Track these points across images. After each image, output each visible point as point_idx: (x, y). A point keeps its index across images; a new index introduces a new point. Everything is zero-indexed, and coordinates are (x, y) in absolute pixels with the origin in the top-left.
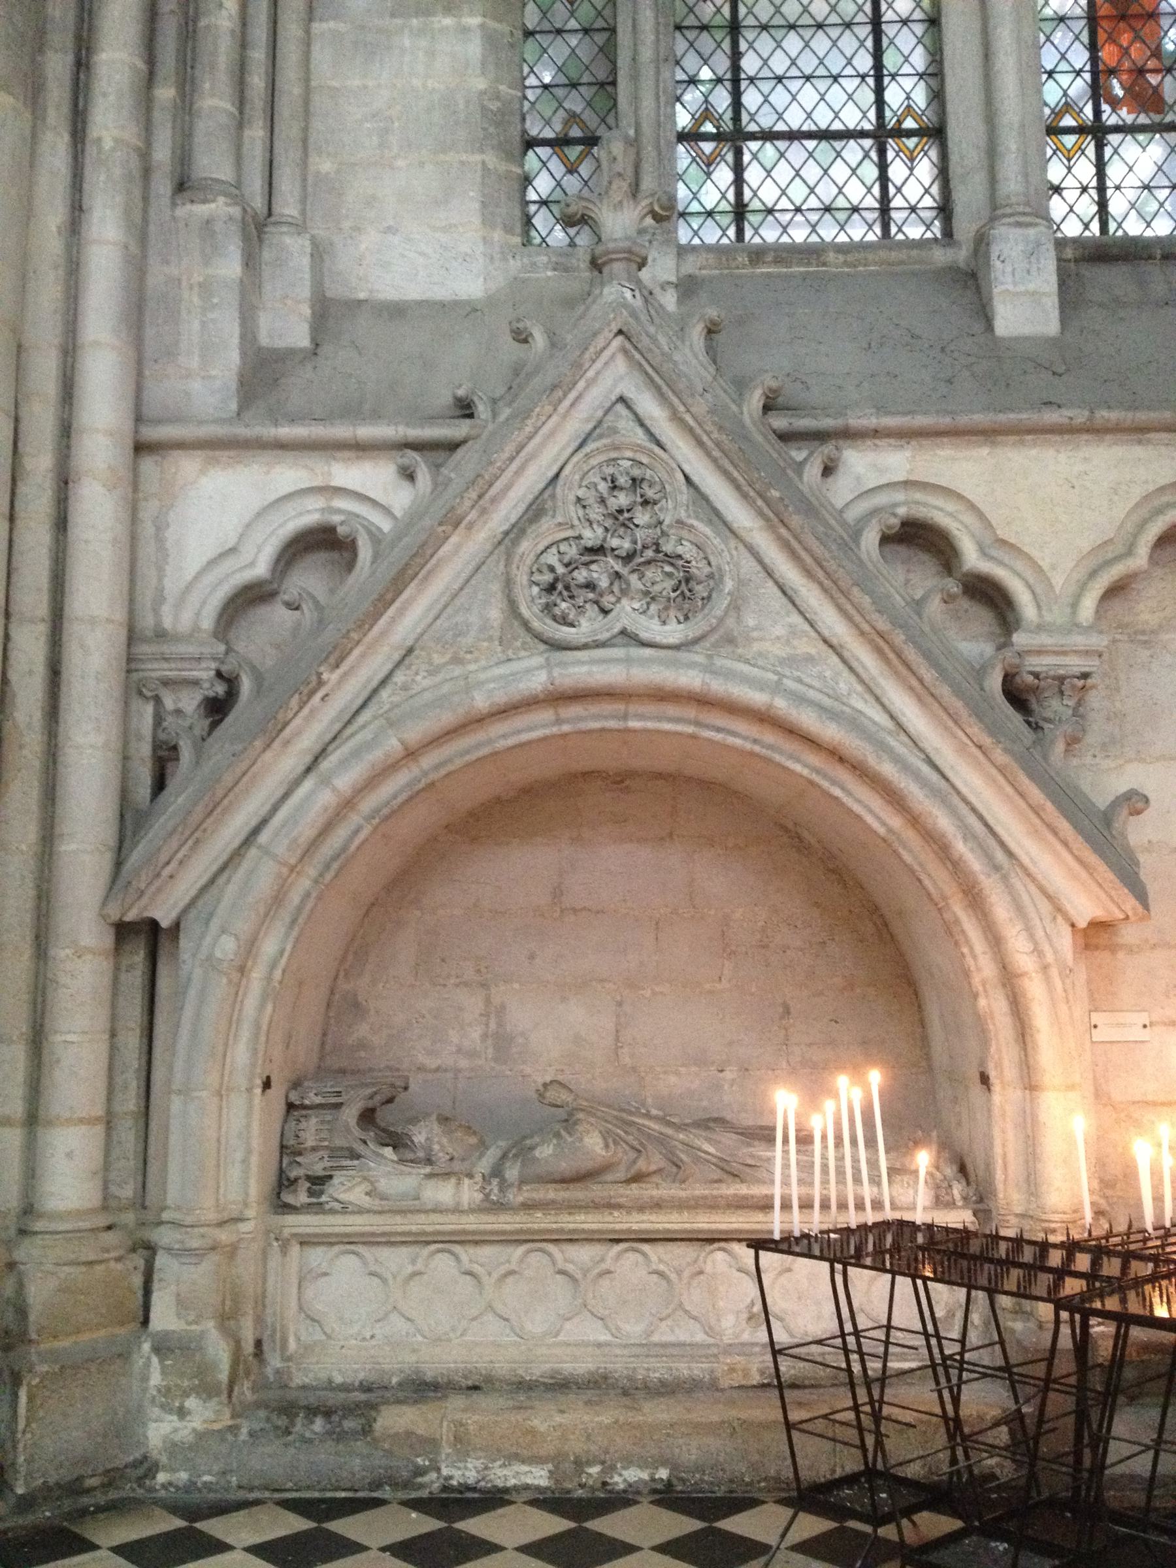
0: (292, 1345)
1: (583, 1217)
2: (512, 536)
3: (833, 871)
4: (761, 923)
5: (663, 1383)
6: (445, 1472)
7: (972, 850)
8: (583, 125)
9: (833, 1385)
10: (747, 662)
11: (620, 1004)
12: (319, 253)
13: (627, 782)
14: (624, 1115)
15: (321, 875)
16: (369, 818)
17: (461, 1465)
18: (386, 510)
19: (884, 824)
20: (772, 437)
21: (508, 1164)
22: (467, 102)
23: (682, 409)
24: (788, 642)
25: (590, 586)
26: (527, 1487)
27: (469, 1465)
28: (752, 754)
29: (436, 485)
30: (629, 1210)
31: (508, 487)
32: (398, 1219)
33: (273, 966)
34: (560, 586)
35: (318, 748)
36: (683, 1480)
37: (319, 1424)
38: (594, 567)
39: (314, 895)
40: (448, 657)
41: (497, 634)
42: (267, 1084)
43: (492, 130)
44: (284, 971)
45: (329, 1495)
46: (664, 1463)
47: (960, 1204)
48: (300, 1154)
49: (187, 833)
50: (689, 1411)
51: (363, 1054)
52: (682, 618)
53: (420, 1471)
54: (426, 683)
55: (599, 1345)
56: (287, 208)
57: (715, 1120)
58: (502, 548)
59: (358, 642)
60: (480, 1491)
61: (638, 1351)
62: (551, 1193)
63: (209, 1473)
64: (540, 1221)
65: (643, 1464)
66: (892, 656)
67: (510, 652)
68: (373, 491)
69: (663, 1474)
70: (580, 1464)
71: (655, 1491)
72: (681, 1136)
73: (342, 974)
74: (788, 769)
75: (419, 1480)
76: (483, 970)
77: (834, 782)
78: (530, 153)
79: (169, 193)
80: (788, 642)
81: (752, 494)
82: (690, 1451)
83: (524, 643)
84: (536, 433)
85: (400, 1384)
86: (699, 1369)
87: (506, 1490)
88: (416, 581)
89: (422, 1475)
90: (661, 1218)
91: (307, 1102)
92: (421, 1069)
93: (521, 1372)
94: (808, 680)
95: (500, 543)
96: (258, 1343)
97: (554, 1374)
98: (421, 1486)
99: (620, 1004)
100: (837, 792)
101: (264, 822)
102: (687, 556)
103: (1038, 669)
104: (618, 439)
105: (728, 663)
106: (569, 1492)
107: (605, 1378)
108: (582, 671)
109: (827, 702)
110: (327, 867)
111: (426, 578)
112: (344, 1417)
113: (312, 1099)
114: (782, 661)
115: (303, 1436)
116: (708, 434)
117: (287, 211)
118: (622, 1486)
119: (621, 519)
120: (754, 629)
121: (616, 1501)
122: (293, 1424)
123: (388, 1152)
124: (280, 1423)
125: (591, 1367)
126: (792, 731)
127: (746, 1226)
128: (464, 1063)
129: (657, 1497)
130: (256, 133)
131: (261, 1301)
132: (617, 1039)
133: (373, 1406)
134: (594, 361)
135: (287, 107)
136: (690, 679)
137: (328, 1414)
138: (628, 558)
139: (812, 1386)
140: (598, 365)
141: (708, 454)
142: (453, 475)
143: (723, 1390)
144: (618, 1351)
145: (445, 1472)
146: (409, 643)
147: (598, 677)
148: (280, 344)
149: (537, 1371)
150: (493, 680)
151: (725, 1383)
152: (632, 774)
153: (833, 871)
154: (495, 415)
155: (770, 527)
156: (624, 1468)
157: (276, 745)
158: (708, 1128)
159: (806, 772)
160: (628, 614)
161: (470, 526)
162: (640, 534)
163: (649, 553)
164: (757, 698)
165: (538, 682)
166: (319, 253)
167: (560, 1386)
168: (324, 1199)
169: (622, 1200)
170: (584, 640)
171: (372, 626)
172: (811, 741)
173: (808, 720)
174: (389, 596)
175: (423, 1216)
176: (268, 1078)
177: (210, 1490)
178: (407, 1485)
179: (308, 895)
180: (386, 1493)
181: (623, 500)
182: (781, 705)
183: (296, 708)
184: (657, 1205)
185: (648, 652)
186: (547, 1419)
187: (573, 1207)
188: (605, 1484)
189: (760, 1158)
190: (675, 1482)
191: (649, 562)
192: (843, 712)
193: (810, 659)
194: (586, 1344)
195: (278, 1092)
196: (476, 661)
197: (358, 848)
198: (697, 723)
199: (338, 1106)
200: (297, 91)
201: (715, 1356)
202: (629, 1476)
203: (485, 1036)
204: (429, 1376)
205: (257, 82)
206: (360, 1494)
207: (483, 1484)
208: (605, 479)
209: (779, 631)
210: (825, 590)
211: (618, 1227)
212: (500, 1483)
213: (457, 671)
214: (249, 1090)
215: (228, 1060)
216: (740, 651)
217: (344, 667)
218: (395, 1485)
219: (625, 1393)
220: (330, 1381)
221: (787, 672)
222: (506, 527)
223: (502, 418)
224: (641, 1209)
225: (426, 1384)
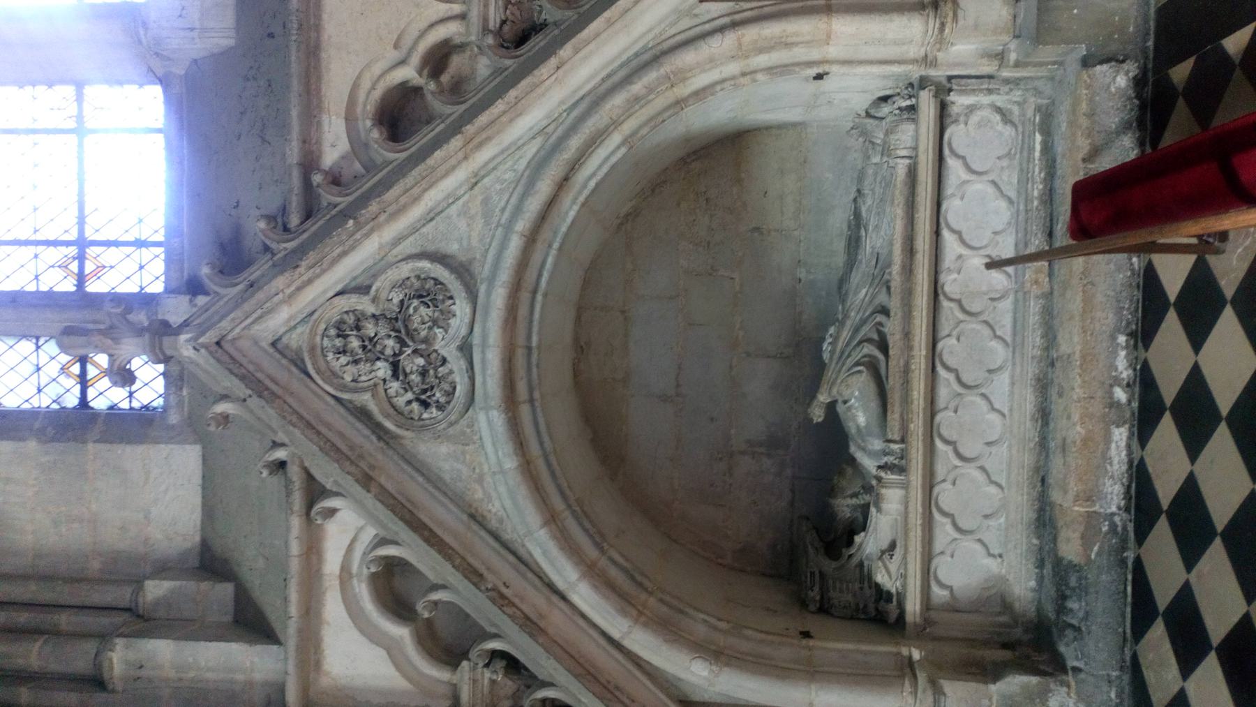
0: (1003, 619)
2: (382, 434)
3: (653, 191)
6: (1114, 509)
7: (640, 78)
11: (748, 354)
15: (646, 590)
16: (602, 551)
19: (618, 148)
20: (309, 222)
21: (870, 447)
22: (47, 453)
24: (472, 218)
25: (423, 373)
26: (1129, 446)
27: (1110, 490)
29: (337, 494)
30: (910, 357)
31: (341, 435)
32: (912, 534)
33: (715, 628)
34: (423, 397)
35: (546, 591)
36: (1129, 323)
37: (1072, 604)
38: (408, 370)
40: (477, 487)
41: (460, 447)
42: (806, 635)
43: (70, 434)
44: (720, 620)
45: (1129, 599)
47: (914, 100)
48: (857, 605)
49: (609, 696)
50: (1071, 318)
53: (1113, 527)
54: (497, 504)
55: (1013, 384)
56: (122, 595)
57: (840, 288)
59: (463, 558)
62: (894, 417)
63: (1108, 692)
64: (917, 426)
65: (1114, 354)
66: (484, 135)
67: (475, 438)
68: (348, 532)
69: (1122, 339)
70: (1114, 405)
71: (1136, 347)
72: (853, 314)
73: (720, 561)
75: (1119, 529)
77: (584, 186)
78: (91, 404)
79: (105, 695)
80: (472, 218)
81: (351, 242)
82: (1106, 318)
83: (468, 426)
85: (1038, 538)
87: (1130, 463)
88: (415, 511)
89: (1116, 526)
90: (918, 331)
91: (818, 598)
92: (792, 503)
93: (1032, 445)
94: (502, 204)
96: (1005, 646)
98: (1125, 528)
99: (748, 354)
100: (592, 184)
101: (604, 634)
102: (401, 296)
103: (498, 21)
105: (487, 267)
106: (1133, 414)
107: (1039, 380)
109: (520, 189)
110: (640, 585)
111: (413, 503)
112: (1067, 585)
113: (815, 594)
114: (487, 223)
117: (128, 596)
119: (370, 348)
120: (461, 245)
121: (1145, 381)
122: (1072, 626)
123: (858, 539)
124: (1071, 637)
125: (1030, 390)
127: (926, 266)
128: (789, 472)
129: (1140, 344)
130: (64, 620)
131: (971, 642)
132: (775, 357)
135: (46, 595)
136: (499, 298)
137: (1064, 597)
143: (1052, 288)
145: (1114, 509)
146: (465, 517)
147: (495, 369)
148: (230, 607)
149: (1033, 434)
150: (496, 452)
152: (576, 339)
153: (653, 191)
154: (283, 445)
155: (379, 227)
156: (1116, 370)
157: (542, 624)
158: (846, 293)
159: (576, 208)
160: (445, 345)
161: (372, 467)
163: (400, 325)
164: (515, 244)
166: (163, 569)
167: (1044, 415)
169: (902, 363)
170: (466, 379)
171: (451, 548)
172: (551, 204)
173: (534, 205)
174: (426, 533)
175: (911, 515)
176: (801, 633)
177: (1123, 692)
179: (661, 600)
180: (1130, 555)
181: (355, 343)
182: (522, 225)
183: (514, 609)
186: (1073, 425)
187: (906, 400)
188: (1128, 385)
190: (1129, 331)
193: (486, 201)
194: (1012, 393)
195: (813, 623)
196: (480, 464)
197: (627, 560)
198: (535, 292)
199: (822, 575)
200: (33, 587)
202: (1123, 366)
203: (769, 456)
204: (1035, 516)
205: (23, 618)
206: (1130, 577)
209: (462, 224)
210: (430, 187)
212: (1125, 468)
213: (488, 479)
216: (478, 256)
217: (482, 570)
219: (1052, 365)
220: (1034, 590)
221: (495, 219)
223: (286, 440)
224: (910, 348)
225: (1038, 519)
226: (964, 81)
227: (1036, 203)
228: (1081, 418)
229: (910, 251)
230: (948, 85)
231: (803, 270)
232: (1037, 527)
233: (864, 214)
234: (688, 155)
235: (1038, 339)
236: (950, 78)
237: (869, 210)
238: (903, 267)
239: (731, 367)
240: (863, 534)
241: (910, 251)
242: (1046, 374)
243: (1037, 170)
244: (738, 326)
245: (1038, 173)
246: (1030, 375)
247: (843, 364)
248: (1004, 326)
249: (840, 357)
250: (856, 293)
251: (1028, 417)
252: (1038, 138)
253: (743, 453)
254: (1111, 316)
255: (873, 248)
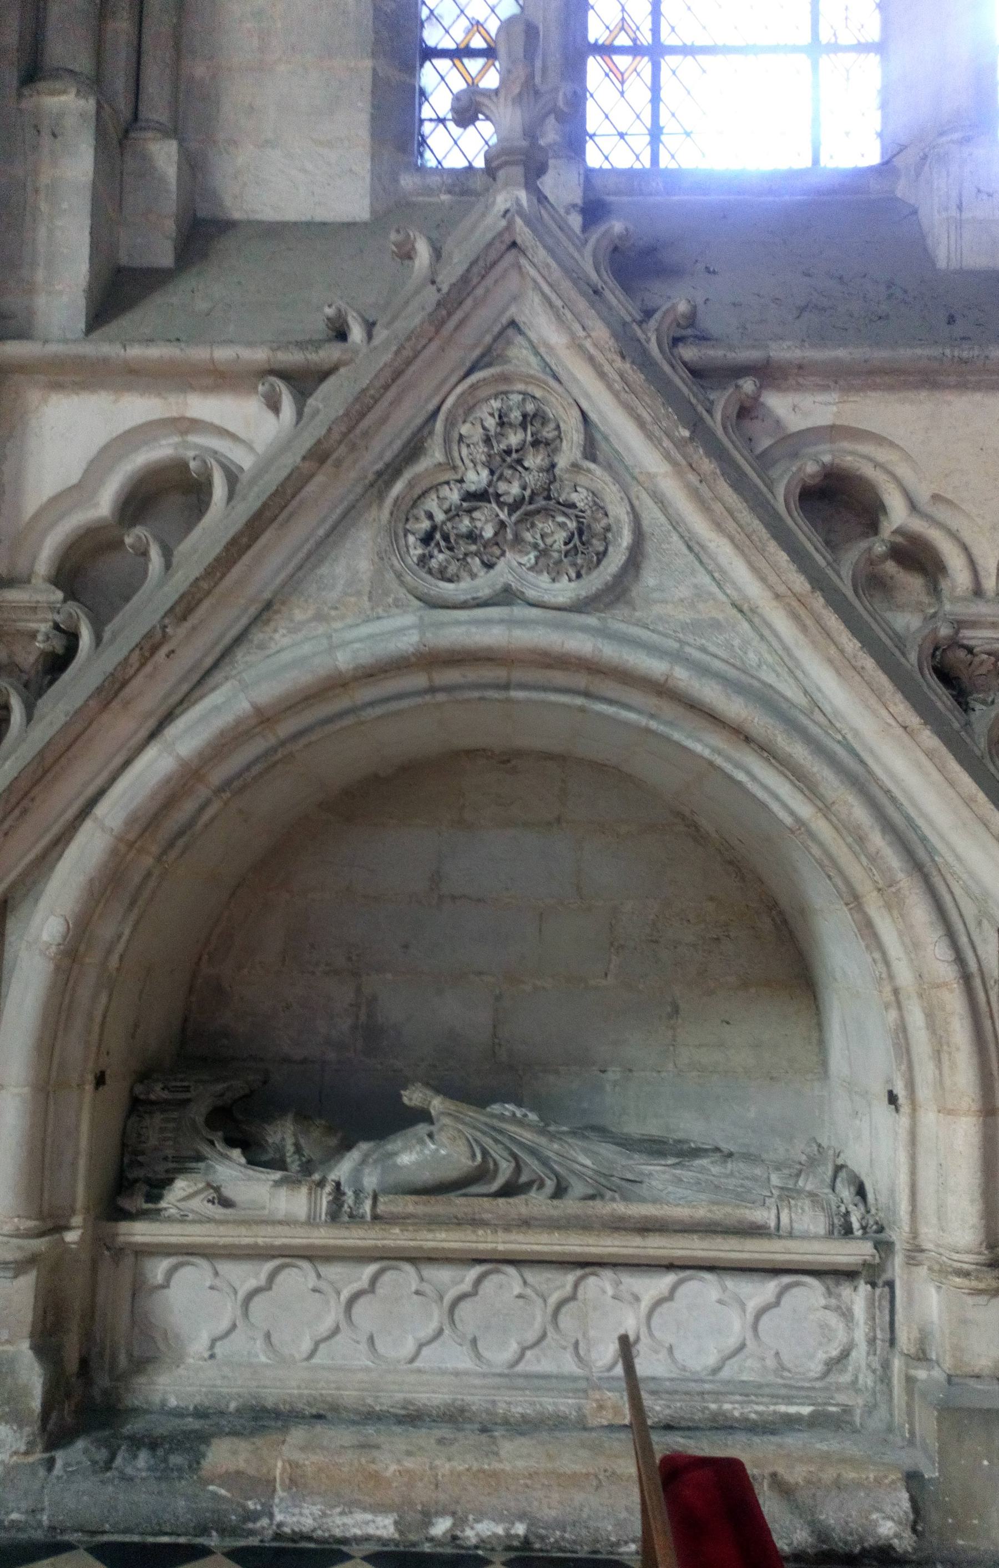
1: (443, 1235)
2: (386, 477)
3: (731, 863)
4: (652, 917)
5: (525, 1419)
6: (279, 1517)
8: (485, 35)
9: (711, 1429)
10: (646, 627)
11: (498, 998)
12: (193, 166)
13: (513, 762)
14: (495, 1123)
17: (297, 1511)
18: (249, 446)
19: (792, 813)
21: (367, 1171)
23: (582, 333)
25: (472, 537)
27: (306, 1512)
28: (648, 730)
29: (300, 414)
31: (384, 420)
32: (243, 1230)
34: (438, 536)
36: (542, 1538)
37: (143, 1458)
38: (476, 514)
39: (156, 872)
40: (310, 613)
42: (100, 1080)
45: (151, 1539)
46: (522, 1517)
47: (859, 1233)
51: (225, 1042)
52: (573, 575)
53: (255, 1516)
55: (457, 1374)
58: (375, 490)
59: (209, 592)
60: (316, 1541)
61: (498, 1380)
62: (409, 1205)
63: (19, 1510)
64: (396, 1238)
66: (809, 622)
67: (380, 610)
69: (520, 1529)
70: (427, 1517)
71: (509, 1548)
73: (206, 957)
74: (685, 748)
75: (250, 1525)
76: (354, 958)
77: (738, 766)
78: (428, 65)
79: (15, 83)
80: (692, 605)
84: (416, 356)
85: (238, 1410)
86: (566, 1405)
87: (345, 1541)
88: (275, 525)
89: (255, 1521)
91: (152, 1097)
92: (286, 1060)
93: (369, 1401)
94: (712, 649)
95: (372, 485)
96: (84, 1363)
97: (406, 1404)
98: (252, 1533)
99: (498, 998)
100: (741, 776)
102: (580, 505)
104: (507, 368)
105: (623, 627)
106: (414, 1544)
107: (462, 1411)
108: (460, 631)
109: (733, 673)
111: (288, 520)
112: (171, 1451)
114: (684, 627)
115: (121, 1472)
116: (611, 362)
117: (155, 117)
118: (474, 1541)
119: (508, 461)
125: (448, 1398)
126: (694, 707)
128: (332, 1055)
131: (90, 1314)
133: (204, 1438)
134: (483, 277)
138: (514, 507)
139: (689, 1429)
140: (489, 281)
141: (609, 387)
142: (321, 406)
144: (477, 1382)
145: (279, 1517)
146: (267, 595)
149: (387, 1401)
151: (593, 1422)
152: (519, 753)
153: (731, 863)
154: (370, 336)
157: (115, 705)
158: (585, 1138)
159: (707, 753)
161: (338, 464)
162: (530, 479)
163: (541, 503)
164: (655, 667)
165: (408, 642)
166: (193, 166)
168: (163, 1204)
169: (486, 1216)
170: (463, 598)
171: (224, 575)
173: (710, 693)
174: (245, 540)
175: (269, 1229)
177: (19, 1530)
178: (234, 1532)
179: (149, 875)
180: (213, 1541)
181: (514, 439)
182: (682, 676)
183: (137, 665)
184: (526, 1224)
185: (535, 612)
186: (397, 1458)
187: (433, 1222)
188: (455, 1538)
189: (642, 1174)
190: (532, 1539)
191: (538, 512)
192: (751, 686)
193: (716, 625)
195: (117, 1090)
196: (343, 618)
199: (185, 1103)
201: (585, 1391)
203: (354, 1028)
204: (269, 1404)
207: (320, 1532)
208: (492, 415)
211: (481, 1246)
212: (338, 1533)
213: (321, 629)
214: (80, 1086)
215: (57, 1053)
216: (637, 614)
217: (193, 620)
218: (222, 1532)
222: (379, 466)
224: (507, 1228)
226: (886, 1304)
227: (713, 1406)
228: (408, 1471)
229: (646, 1228)
230: (880, 1282)
231: (618, 1076)
232: (252, 1408)
233: (698, 1162)
234: (781, 913)
235: (520, 1410)
236: (890, 1285)
237: (703, 1170)
238: (622, 1219)
239: (480, 973)
240: (243, 1160)
241: (646, 1228)
242: (470, 1421)
243: (760, 1408)
244: (539, 983)
245: (755, 1410)
246: (468, 1398)
247: (484, 1133)
248: (539, 1361)
249: (494, 1129)
250: (585, 1151)
251: (409, 1396)
252: (806, 1410)
253: (358, 990)
254: (553, 1513)
255: (650, 1175)
